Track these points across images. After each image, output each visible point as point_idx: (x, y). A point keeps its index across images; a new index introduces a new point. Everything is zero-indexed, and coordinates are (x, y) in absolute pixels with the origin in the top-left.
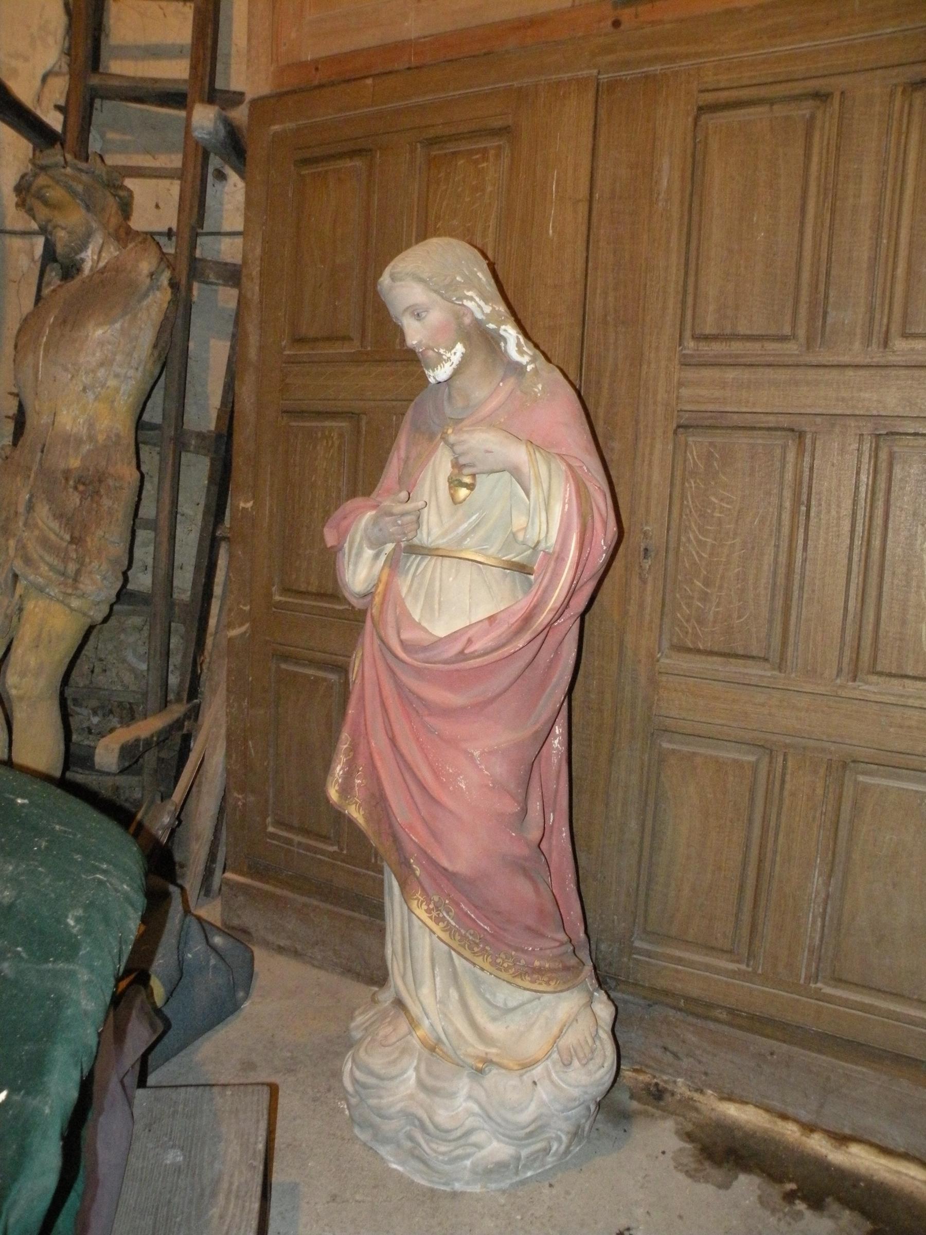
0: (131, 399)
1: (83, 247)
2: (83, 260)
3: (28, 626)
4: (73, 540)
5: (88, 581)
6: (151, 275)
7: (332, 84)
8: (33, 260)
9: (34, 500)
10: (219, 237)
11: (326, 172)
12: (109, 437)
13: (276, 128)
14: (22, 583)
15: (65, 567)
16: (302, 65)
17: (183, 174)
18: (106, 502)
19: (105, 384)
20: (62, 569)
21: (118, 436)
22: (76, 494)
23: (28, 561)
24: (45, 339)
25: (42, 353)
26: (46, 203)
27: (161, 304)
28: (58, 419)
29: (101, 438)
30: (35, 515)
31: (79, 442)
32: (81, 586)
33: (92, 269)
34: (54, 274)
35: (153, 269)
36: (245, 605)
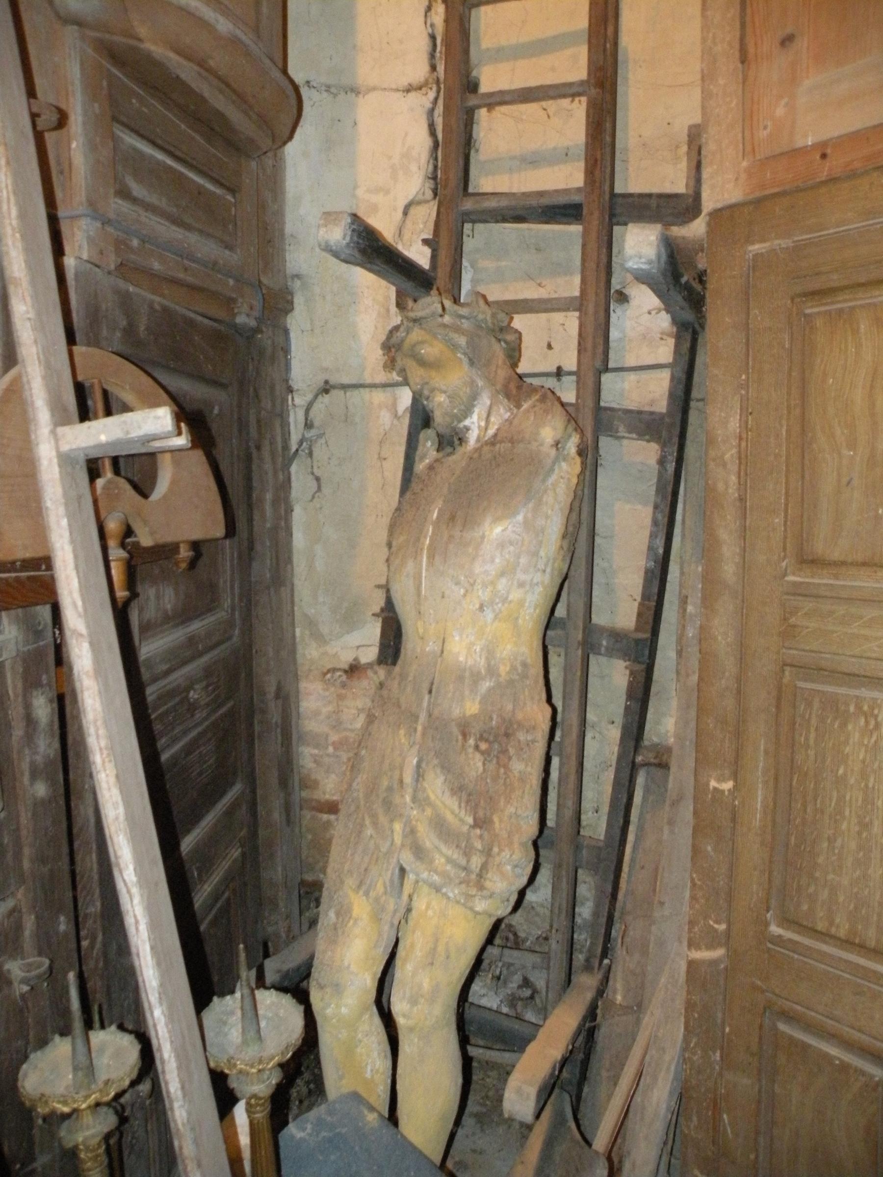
0: (537, 611)
1: (467, 412)
2: (467, 429)
3: (418, 933)
4: (477, 824)
5: (496, 878)
6: (557, 444)
7: (853, 175)
8: (396, 416)
9: (424, 765)
10: (621, 374)
11: (852, 308)
12: (513, 668)
13: (756, 248)
14: (411, 877)
15: (468, 861)
16: (795, 153)
17: (581, 305)
18: (517, 766)
19: (507, 598)
20: (463, 862)
21: (524, 665)
22: (478, 756)
23: (419, 852)
24: (428, 542)
25: (425, 559)
26: (423, 363)
27: (569, 479)
28: (448, 647)
29: (503, 670)
30: (426, 785)
31: (476, 678)
32: (488, 884)
33: (478, 440)
34: (429, 444)
35: (558, 437)
36: (717, 922)
